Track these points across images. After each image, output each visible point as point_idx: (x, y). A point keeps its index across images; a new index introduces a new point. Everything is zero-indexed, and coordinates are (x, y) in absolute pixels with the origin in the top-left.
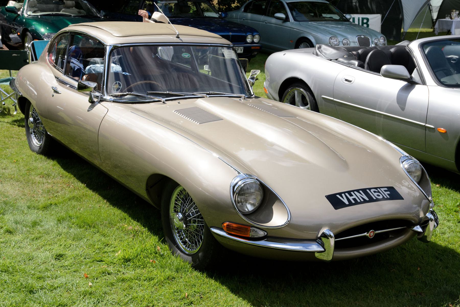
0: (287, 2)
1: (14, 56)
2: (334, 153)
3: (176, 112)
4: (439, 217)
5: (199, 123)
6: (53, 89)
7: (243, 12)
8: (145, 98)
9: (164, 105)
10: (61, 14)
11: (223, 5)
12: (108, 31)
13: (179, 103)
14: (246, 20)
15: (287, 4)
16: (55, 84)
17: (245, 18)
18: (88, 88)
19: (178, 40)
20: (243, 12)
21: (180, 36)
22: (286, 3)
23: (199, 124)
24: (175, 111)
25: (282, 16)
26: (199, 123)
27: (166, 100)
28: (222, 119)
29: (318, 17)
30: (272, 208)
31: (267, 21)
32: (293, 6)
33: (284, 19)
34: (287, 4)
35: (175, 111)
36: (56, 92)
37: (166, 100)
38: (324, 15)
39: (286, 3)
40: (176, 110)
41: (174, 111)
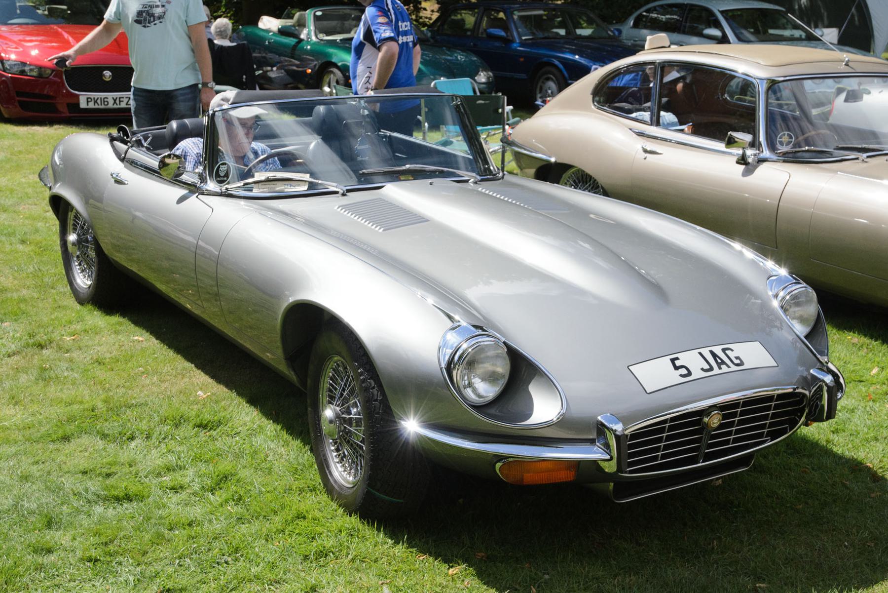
0: (721, 10)
1: (479, 104)
2: (629, 268)
3: (340, 208)
4: (116, 493)
5: (382, 229)
6: (113, 177)
7: (631, 28)
8: (832, 154)
9: (865, 165)
10: (338, 35)
11: (278, 12)
12: (748, 59)
13: (431, 184)
14: (640, 40)
15: (722, 12)
16: (639, 144)
17: (637, 38)
18: (736, 142)
19: (848, 69)
20: (631, 28)
21: (850, 64)
22: (719, 10)
23: (384, 230)
24: (338, 208)
25: (716, 32)
26: (382, 229)
27: (868, 157)
28: (427, 221)
29: (762, 33)
30: (529, 391)
31: (637, 38)
32: (732, 16)
33: (720, 38)
34: (722, 12)
35: (338, 208)
36: (119, 182)
37: (868, 157)
38: (771, 31)
39: (719, 10)
40: (341, 204)
41: (337, 207)
